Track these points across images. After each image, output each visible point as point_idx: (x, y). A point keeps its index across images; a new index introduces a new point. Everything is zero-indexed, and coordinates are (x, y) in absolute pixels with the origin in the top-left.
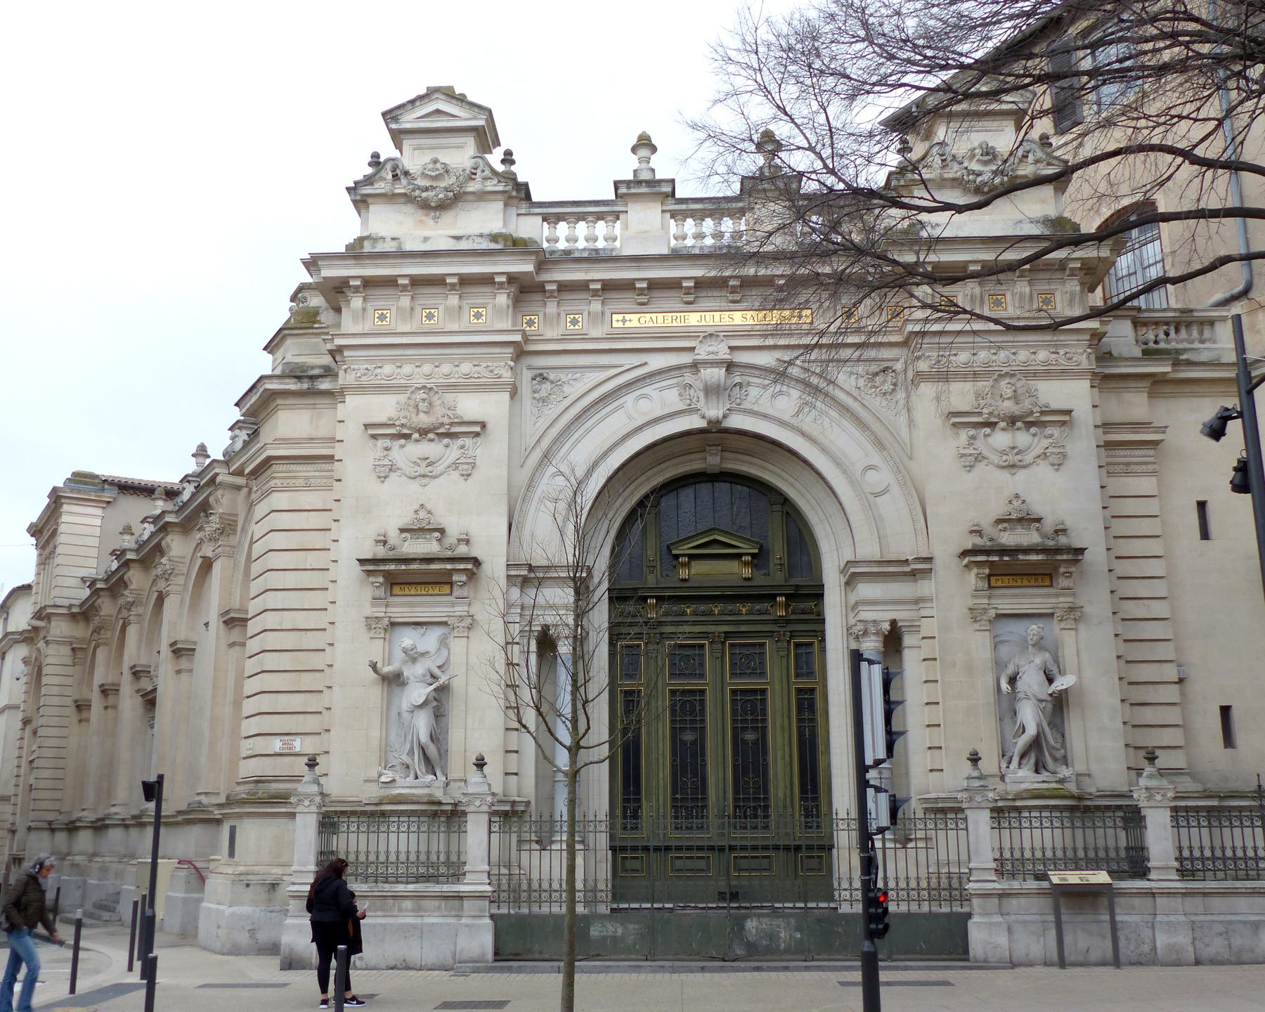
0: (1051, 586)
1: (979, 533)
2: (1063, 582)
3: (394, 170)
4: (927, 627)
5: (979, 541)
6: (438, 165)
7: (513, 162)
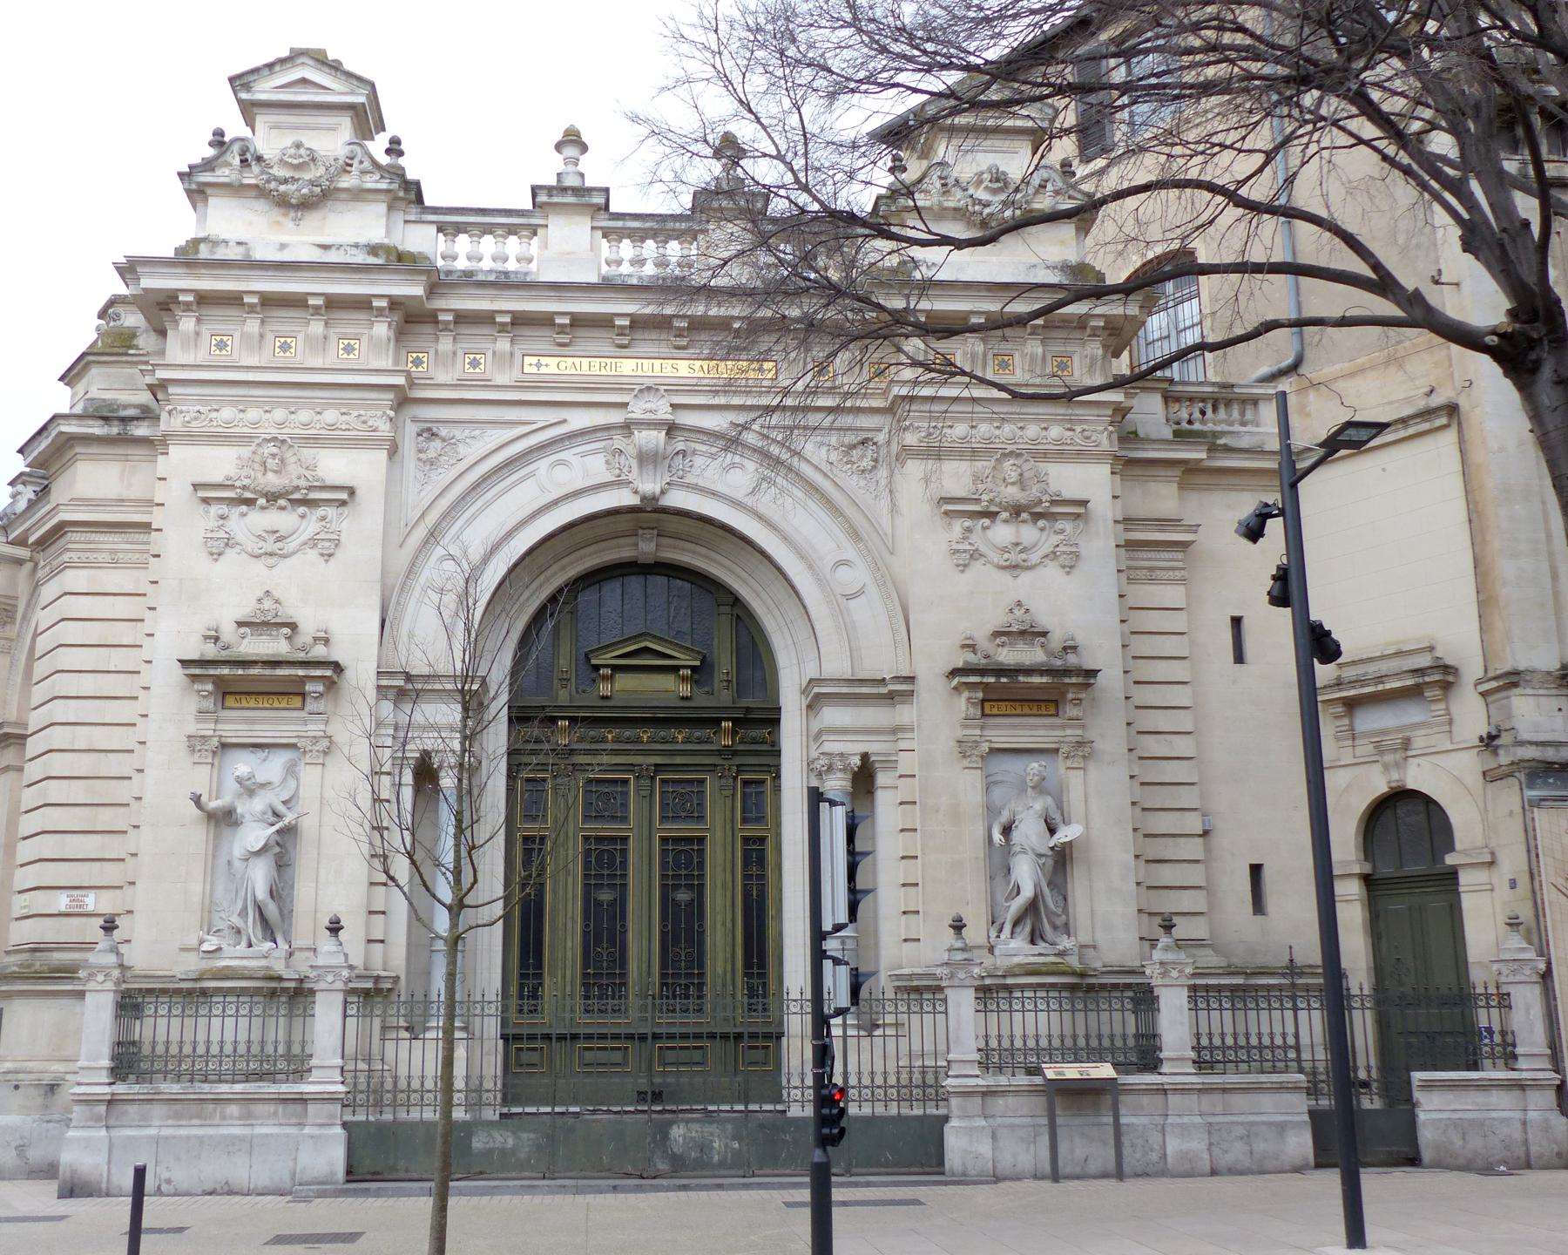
1: (972, 647)
2: (1071, 711)
3: (243, 152)
4: (906, 763)
5: (971, 658)
6: (302, 151)
7: (401, 153)
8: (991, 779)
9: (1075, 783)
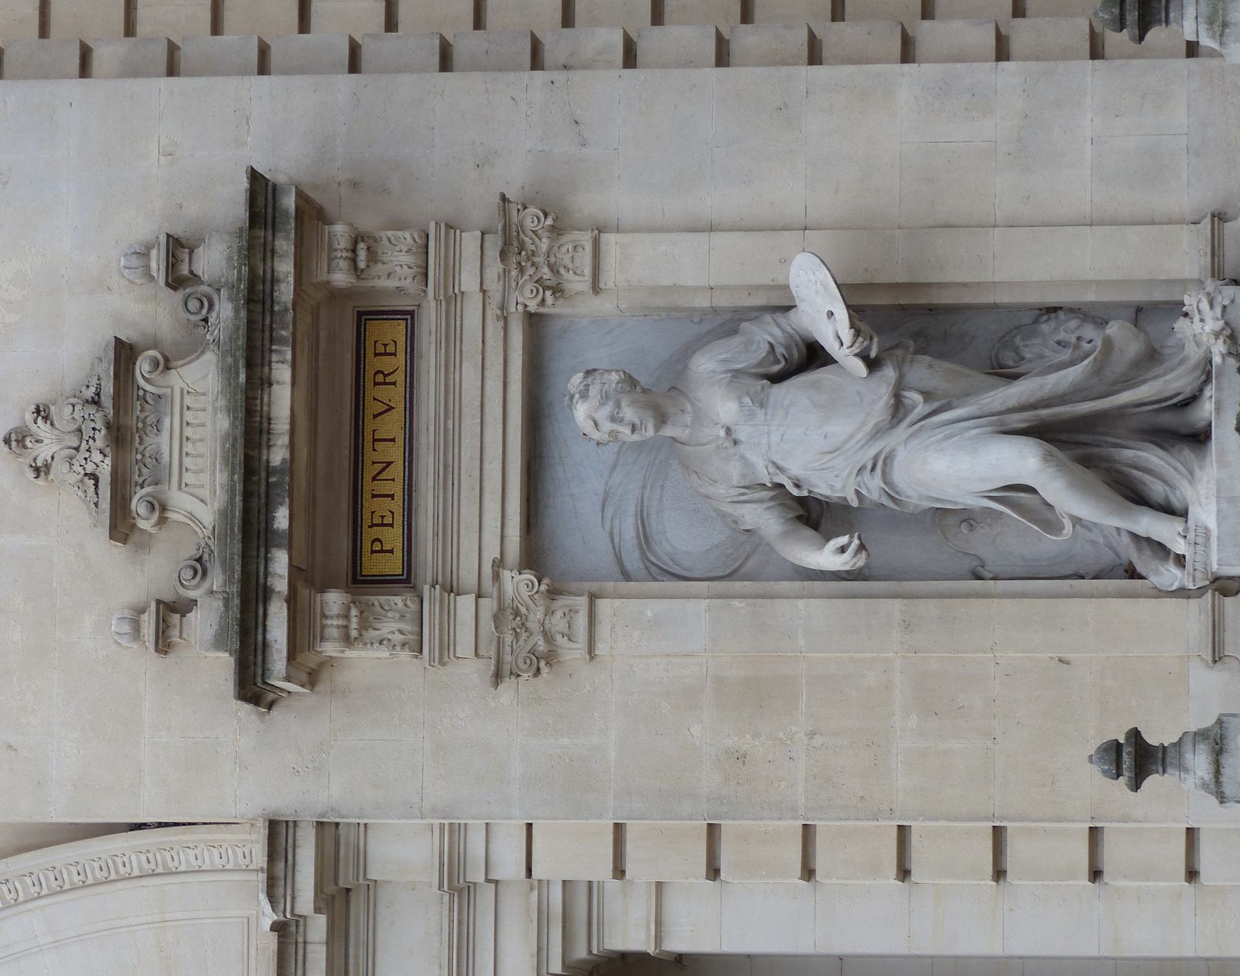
0: (409, 317)
1: (171, 611)
2: (395, 273)
4: (572, 854)
5: (205, 621)
8: (633, 561)
9: (647, 266)
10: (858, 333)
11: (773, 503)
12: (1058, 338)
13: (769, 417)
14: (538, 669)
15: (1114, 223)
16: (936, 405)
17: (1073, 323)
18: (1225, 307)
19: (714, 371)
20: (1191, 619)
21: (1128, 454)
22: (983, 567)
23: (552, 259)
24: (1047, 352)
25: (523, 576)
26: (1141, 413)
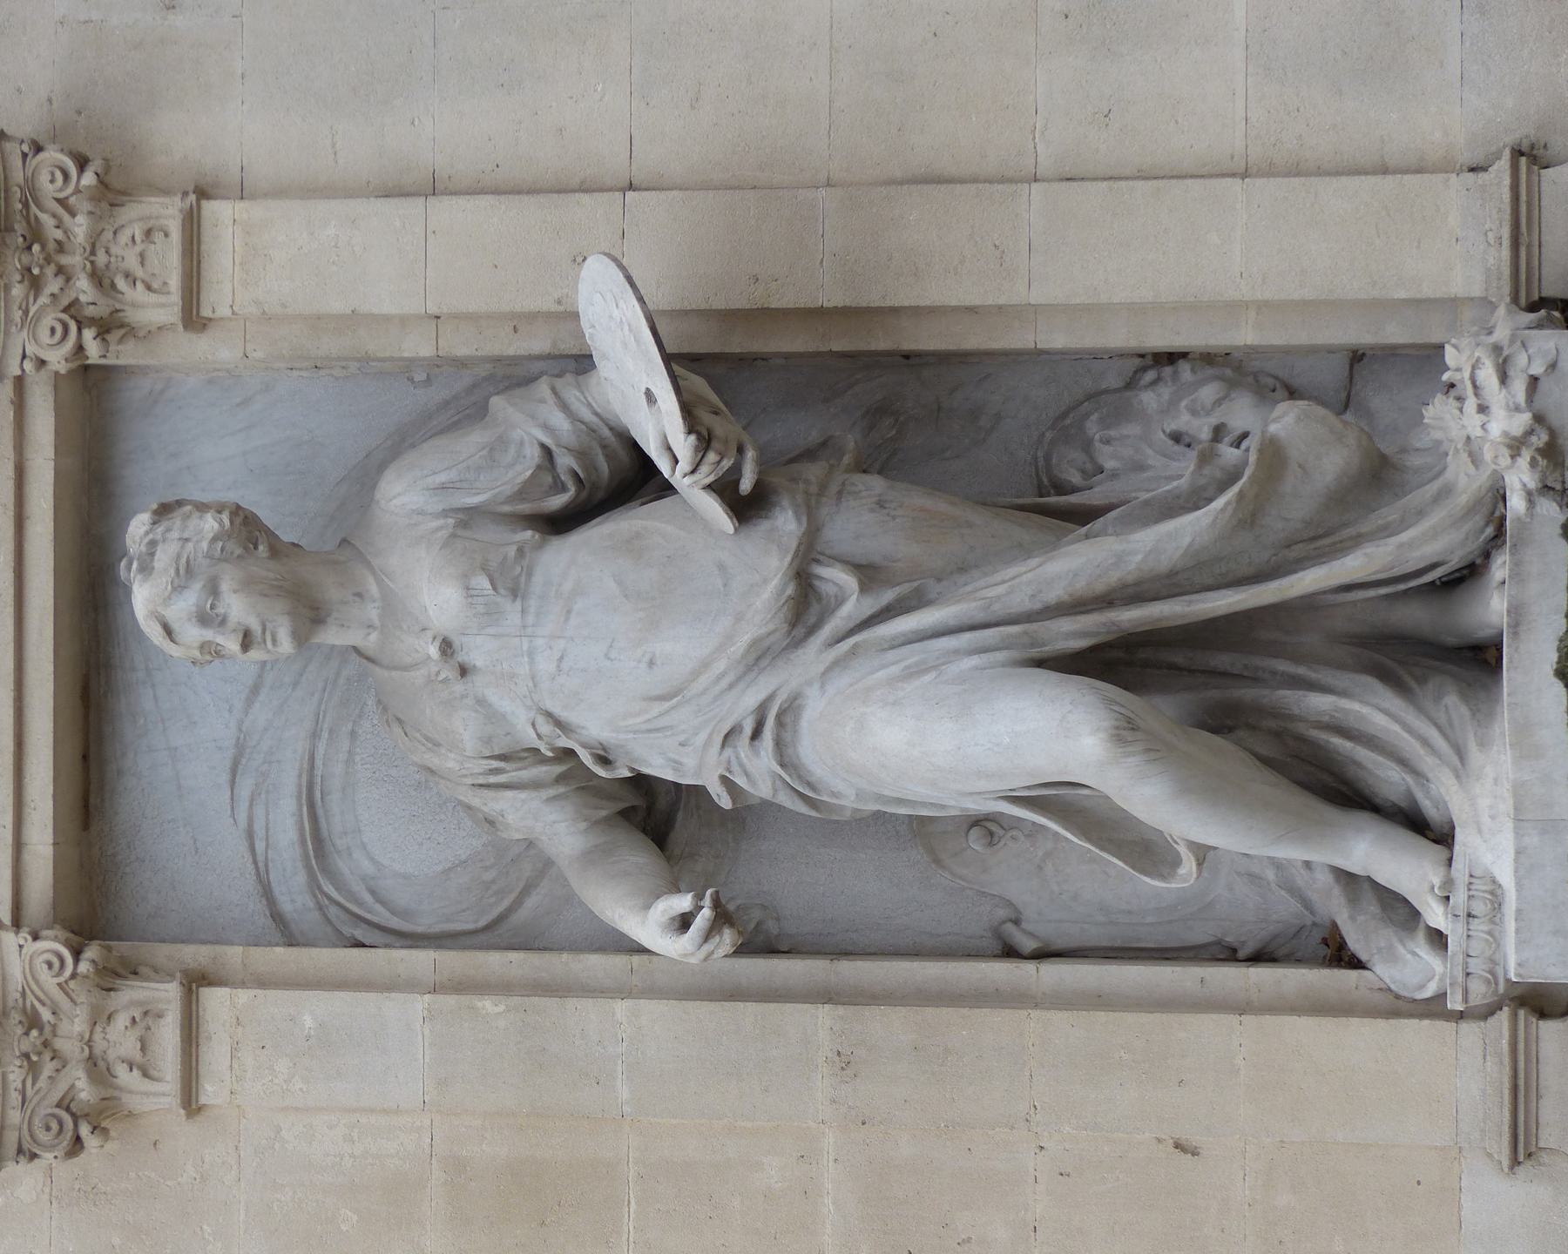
8: (294, 895)
10: (705, 442)
11: (561, 789)
12: (1172, 426)
13: (530, 619)
14: (78, 1139)
15: (1296, 171)
16: (888, 596)
17: (1209, 392)
18: (1534, 381)
19: (421, 513)
20: (1467, 1064)
21: (1319, 703)
22: (1017, 922)
23: (101, 258)
24: (1154, 460)
25: (42, 945)
26: (1354, 603)
